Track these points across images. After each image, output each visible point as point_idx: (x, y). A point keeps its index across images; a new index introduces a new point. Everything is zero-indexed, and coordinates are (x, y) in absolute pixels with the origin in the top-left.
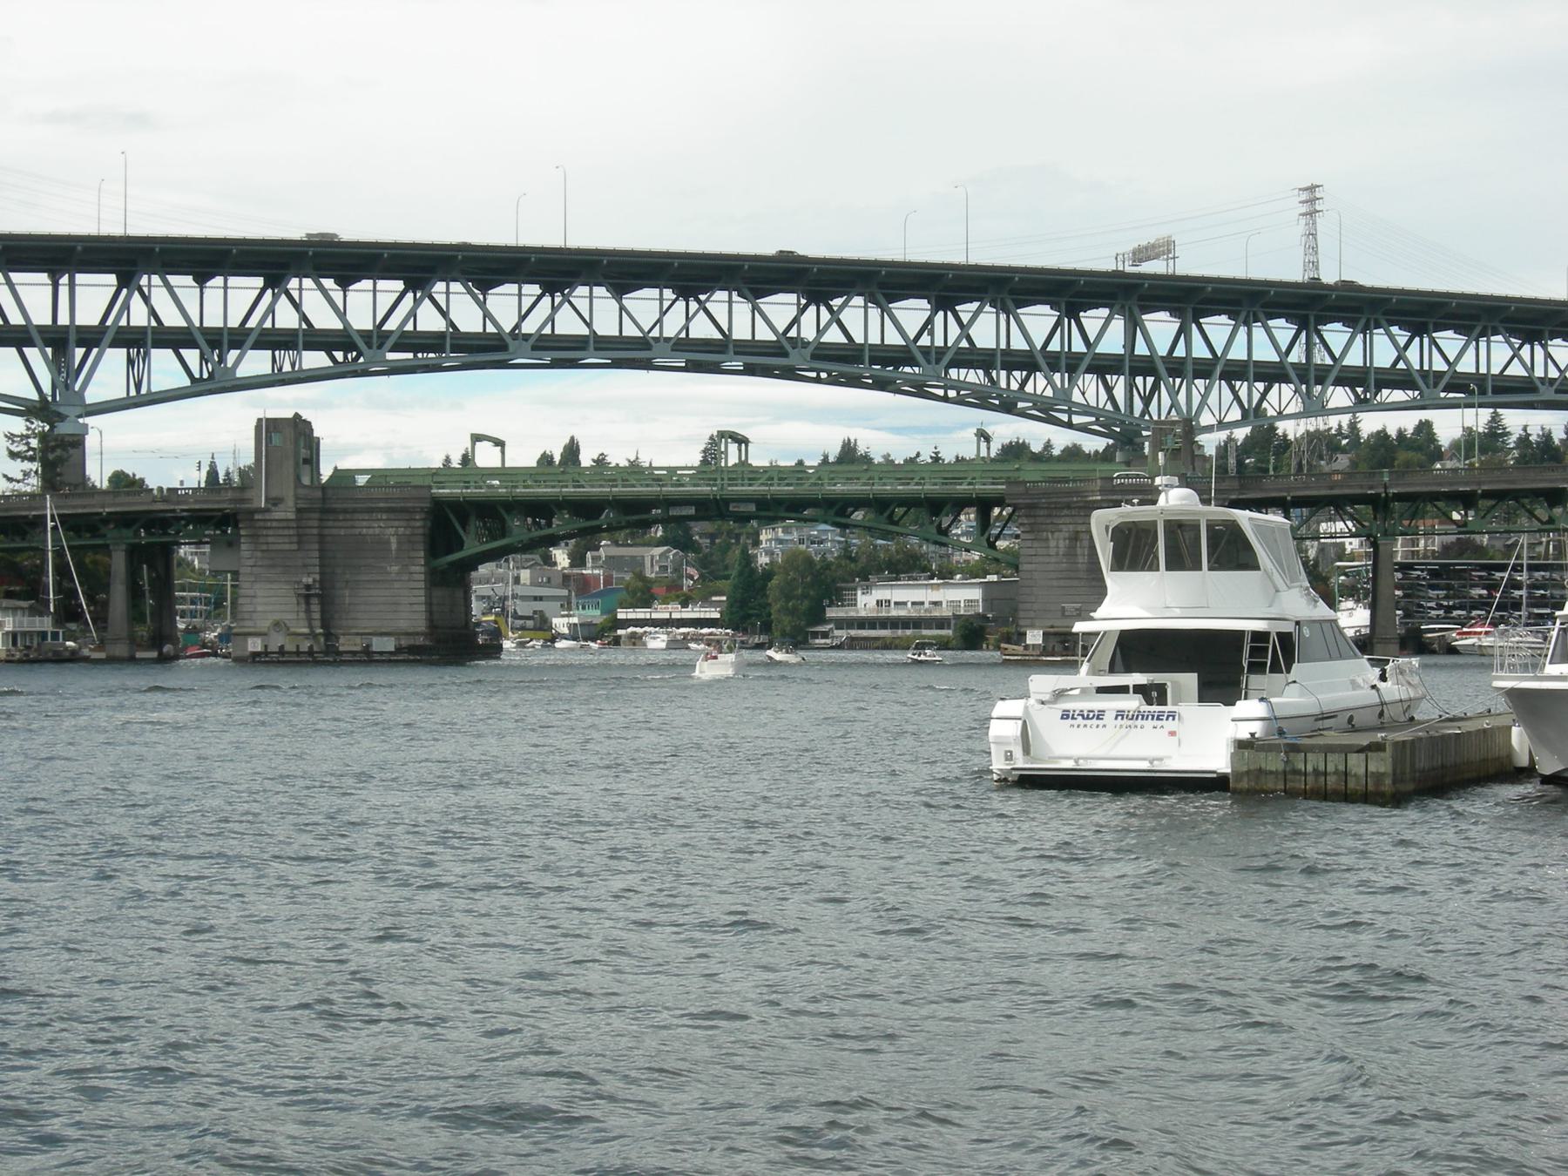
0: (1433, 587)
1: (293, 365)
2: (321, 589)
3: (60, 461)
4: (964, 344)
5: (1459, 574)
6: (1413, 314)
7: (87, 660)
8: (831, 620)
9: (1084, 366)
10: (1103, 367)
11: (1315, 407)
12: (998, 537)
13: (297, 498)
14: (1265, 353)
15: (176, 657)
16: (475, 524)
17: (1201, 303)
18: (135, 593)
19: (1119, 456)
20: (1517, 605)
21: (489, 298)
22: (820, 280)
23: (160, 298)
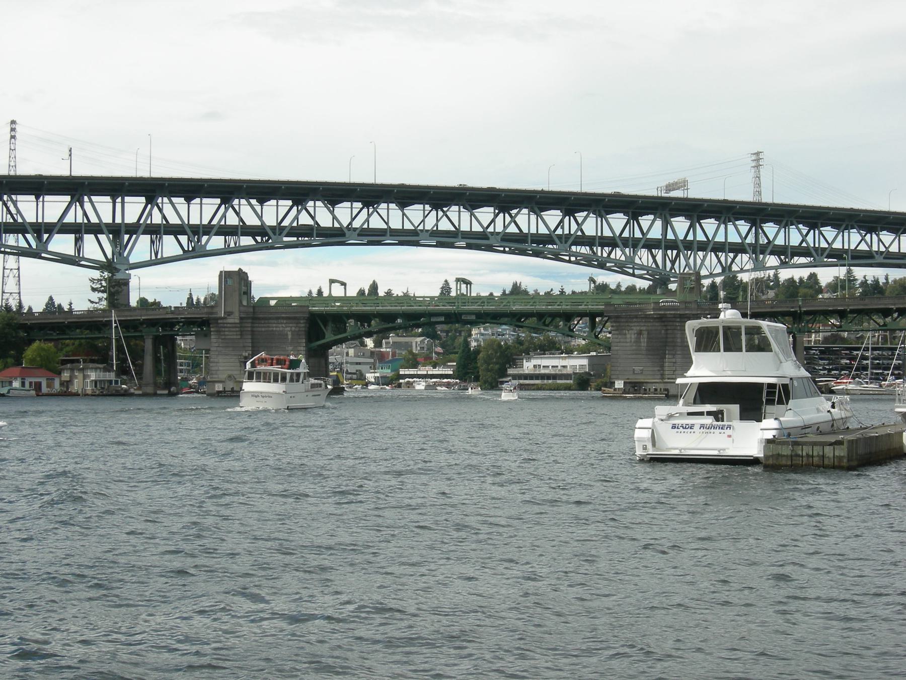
0: (822, 359)
1: (235, 244)
3: (118, 292)
4: (579, 233)
5: (835, 352)
6: (811, 218)
7: (132, 395)
8: (510, 375)
9: (641, 244)
10: (651, 245)
11: (759, 266)
14: (734, 238)
15: (178, 393)
16: (330, 326)
17: (702, 212)
18: (157, 360)
19: (659, 291)
20: (865, 368)
21: (264, 207)
22: (505, 200)
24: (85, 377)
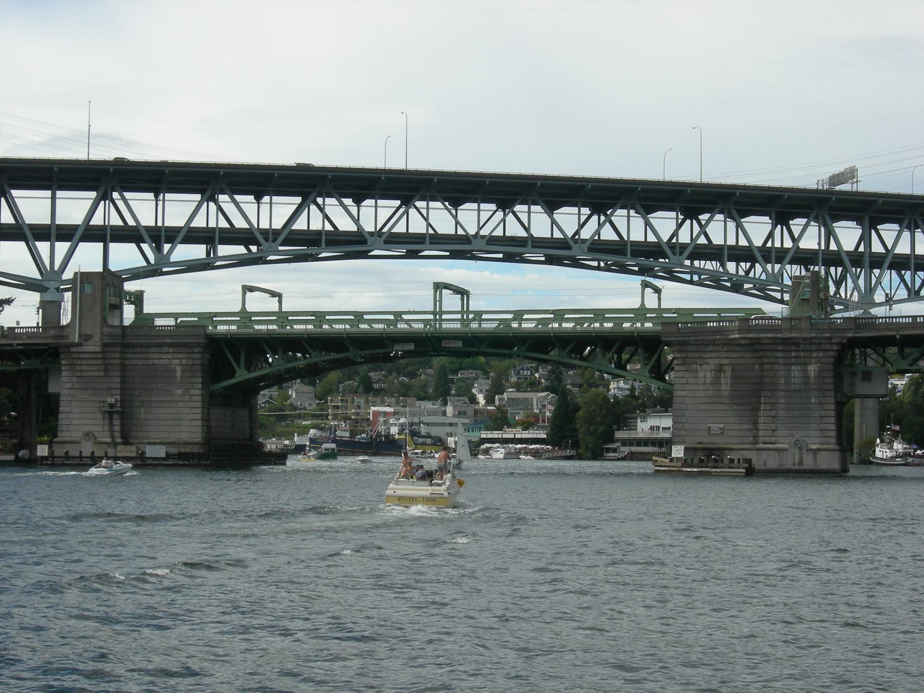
2: (122, 407)
4: (702, 240)
8: (618, 440)
10: (804, 258)
12: (628, 361)
13: (102, 335)
21: (362, 209)
23: (230, 208)
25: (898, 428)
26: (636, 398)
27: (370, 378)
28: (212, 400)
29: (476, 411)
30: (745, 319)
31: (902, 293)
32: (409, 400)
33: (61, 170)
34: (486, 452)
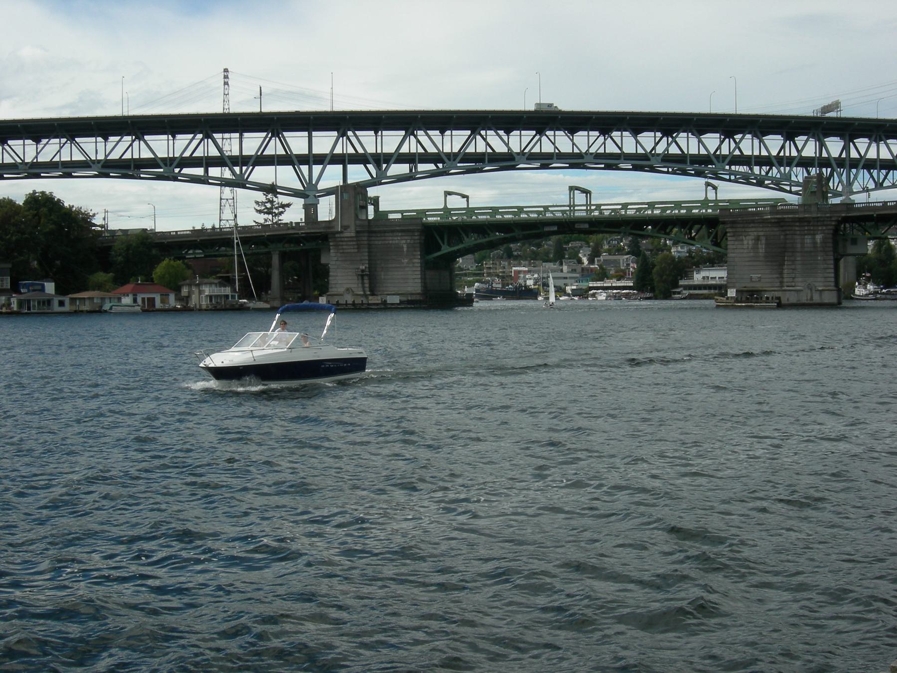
4: (737, 153)
8: (681, 286)
10: (805, 163)
13: (356, 226)
22: (668, 124)
23: (423, 139)
24: (200, 292)
25: (868, 275)
26: (693, 258)
27: (511, 248)
28: (427, 266)
29: (583, 269)
30: (774, 205)
31: (871, 185)
32: (537, 262)
33: (315, 118)
34: (594, 295)
